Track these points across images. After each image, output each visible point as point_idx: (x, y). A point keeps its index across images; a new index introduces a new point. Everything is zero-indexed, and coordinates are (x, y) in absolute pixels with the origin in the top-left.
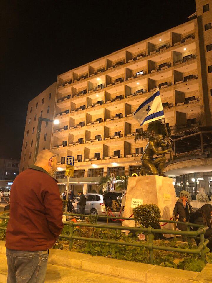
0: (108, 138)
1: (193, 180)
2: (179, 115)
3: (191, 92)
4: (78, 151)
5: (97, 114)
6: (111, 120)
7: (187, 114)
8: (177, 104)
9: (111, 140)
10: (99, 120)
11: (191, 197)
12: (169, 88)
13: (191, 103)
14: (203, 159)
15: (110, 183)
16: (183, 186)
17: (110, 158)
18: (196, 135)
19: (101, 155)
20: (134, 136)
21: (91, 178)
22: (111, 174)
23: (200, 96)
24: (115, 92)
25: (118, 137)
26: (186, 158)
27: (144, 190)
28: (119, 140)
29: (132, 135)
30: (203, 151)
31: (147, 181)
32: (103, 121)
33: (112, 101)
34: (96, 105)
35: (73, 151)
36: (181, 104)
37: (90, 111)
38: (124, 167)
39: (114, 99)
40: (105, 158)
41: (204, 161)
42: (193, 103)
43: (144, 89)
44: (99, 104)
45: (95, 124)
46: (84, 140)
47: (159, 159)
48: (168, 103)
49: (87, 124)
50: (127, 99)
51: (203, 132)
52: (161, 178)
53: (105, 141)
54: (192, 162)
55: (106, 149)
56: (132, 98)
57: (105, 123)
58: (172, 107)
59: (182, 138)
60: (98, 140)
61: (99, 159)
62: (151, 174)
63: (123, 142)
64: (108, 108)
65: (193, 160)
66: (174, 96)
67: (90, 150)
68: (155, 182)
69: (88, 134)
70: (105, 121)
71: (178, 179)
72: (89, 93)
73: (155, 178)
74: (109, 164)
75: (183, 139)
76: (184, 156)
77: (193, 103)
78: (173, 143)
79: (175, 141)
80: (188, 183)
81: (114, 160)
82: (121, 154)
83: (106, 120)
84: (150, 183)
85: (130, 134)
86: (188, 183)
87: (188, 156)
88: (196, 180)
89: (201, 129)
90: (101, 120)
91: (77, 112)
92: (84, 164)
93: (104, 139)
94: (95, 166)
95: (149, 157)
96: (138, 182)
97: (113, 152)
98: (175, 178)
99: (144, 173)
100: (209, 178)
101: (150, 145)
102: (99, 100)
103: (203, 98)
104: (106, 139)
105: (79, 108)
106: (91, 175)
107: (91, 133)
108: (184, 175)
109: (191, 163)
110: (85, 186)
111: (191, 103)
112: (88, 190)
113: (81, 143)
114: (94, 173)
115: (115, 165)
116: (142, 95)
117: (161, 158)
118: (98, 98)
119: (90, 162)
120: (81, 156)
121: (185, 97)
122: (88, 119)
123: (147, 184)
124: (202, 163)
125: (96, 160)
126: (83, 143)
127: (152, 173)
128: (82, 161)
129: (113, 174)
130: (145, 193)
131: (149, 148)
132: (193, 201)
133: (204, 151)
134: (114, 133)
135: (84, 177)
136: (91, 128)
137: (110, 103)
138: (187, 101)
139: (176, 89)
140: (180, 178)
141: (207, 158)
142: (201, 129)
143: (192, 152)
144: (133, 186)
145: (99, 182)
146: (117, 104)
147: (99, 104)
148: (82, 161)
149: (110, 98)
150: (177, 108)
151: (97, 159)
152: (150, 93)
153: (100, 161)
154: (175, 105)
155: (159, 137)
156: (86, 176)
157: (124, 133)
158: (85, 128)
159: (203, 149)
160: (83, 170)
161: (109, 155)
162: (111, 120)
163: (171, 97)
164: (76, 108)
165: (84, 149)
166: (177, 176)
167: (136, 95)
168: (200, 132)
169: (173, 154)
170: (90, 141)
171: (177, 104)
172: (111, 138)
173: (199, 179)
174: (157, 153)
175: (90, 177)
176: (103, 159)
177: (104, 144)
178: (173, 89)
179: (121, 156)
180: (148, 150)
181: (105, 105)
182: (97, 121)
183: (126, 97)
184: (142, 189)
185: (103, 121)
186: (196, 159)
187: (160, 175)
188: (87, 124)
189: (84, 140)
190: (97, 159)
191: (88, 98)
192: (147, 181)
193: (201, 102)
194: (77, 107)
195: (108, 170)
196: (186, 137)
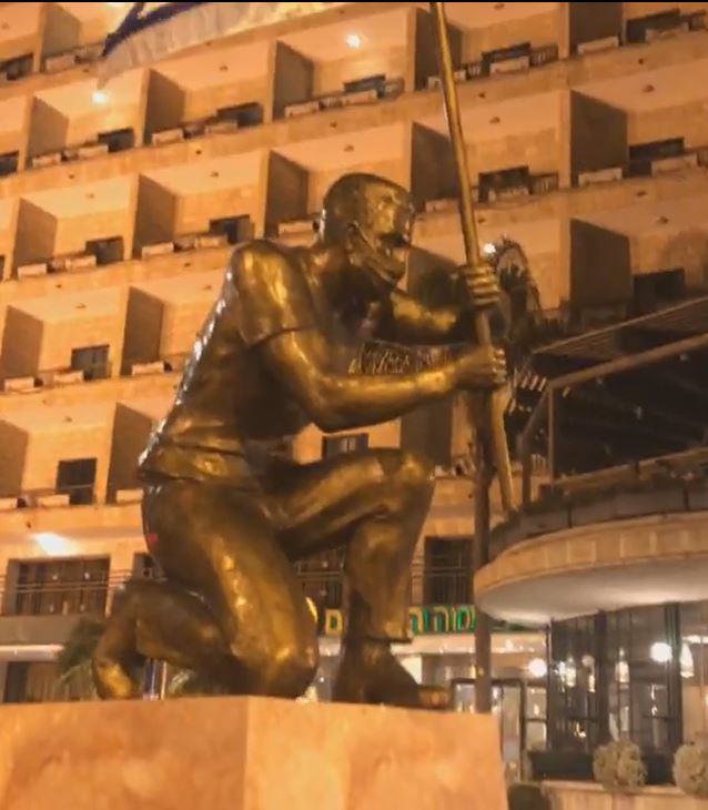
1: (660, 652)
2: (594, 249)
8: (582, 178)
10: (104, 252)
11: (638, 764)
12: (536, 74)
16: (592, 679)
24: (218, 79)
26: (622, 505)
35: (35, 432)
36: (605, 175)
37: (42, 186)
38: (104, 563)
42: (671, 173)
43: (392, 75)
44: (106, 148)
47: (339, 483)
49: (22, 271)
50: (283, 128)
54: (660, 534)
61: (81, 497)
62: (229, 674)
65: (670, 516)
70: (136, 254)
71: (562, 640)
72: (43, 70)
75: (609, 378)
76: (610, 493)
77: (671, 173)
78: (547, 399)
79: (558, 391)
80: (623, 669)
86: (623, 669)
87: (637, 490)
88: (677, 653)
93: (126, 372)
94: (52, 545)
95: (233, 445)
97: (56, 464)
98: (545, 629)
99: (147, 648)
102: (111, 124)
104: (137, 369)
108: (601, 618)
109: (653, 538)
114: (47, 589)
116: (375, 111)
118: (107, 111)
119: (19, 518)
125: (63, 506)
127: (236, 651)
132: (654, 789)
138: (639, 161)
140: (578, 633)
143: (661, 463)
145: (59, 653)
153: (84, 513)
154: (565, 181)
163: (544, 138)
166: (560, 617)
169: (540, 479)
174: (327, 391)
180: (226, 360)
188: (22, 271)
190: (65, 499)
191: (37, 108)
195: (16, 574)
196: (624, 362)
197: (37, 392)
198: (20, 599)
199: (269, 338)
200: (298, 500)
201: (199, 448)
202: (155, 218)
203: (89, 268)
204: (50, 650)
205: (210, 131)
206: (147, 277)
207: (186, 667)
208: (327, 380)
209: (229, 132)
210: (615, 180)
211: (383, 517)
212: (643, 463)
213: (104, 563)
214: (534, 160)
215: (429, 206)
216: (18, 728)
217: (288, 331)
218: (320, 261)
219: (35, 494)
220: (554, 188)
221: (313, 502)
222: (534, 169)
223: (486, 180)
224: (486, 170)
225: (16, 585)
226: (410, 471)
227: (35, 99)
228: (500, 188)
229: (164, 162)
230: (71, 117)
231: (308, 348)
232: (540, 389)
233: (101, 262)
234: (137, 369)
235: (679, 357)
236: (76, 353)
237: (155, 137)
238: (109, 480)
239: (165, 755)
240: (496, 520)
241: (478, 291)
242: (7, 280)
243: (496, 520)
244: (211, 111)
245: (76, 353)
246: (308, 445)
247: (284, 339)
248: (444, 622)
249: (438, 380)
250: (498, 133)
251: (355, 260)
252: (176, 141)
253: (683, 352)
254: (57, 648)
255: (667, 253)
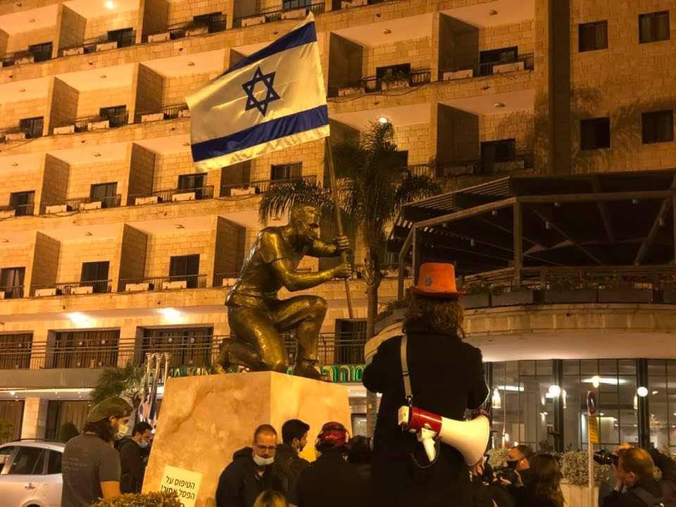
0: (148, 200)
2: (453, 124)
3: (507, 29)
4: (8, 250)
5: (105, 84)
6: (166, 117)
7: (480, 119)
9: (162, 208)
10: (114, 117)
13: (501, 74)
14: (519, 308)
15: (143, 398)
17: (151, 287)
18: (500, 210)
19: (114, 274)
20: (260, 199)
21: (61, 372)
22: (150, 357)
23: (538, 48)
25: (193, 195)
27: (222, 434)
28: (194, 211)
29: (252, 190)
30: (518, 277)
31: (238, 395)
32: (131, 120)
33: (174, 37)
34: (99, 46)
35: (66, 242)
36: (461, 74)
37: (70, 69)
38: (116, 333)
39: (185, 29)
40: (129, 287)
41: (520, 316)
44: (115, 44)
45: (92, 131)
46: (37, 199)
47: (294, 308)
48: (409, 65)
49: (56, 131)
51: (526, 198)
52: (299, 383)
53: (133, 212)
55: (135, 247)
56: (263, 28)
57: (139, 131)
58: (422, 83)
59: (445, 218)
60: (99, 204)
61: (100, 289)
62: (258, 366)
63: (213, 219)
64: (156, 65)
65: (480, 311)
66: (437, 39)
67: (63, 249)
68: (268, 398)
69: (55, 173)
70: (137, 120)
73: (268, 385)
74: (145, 311)
75: (450, 223)
78: (412, 234)
79: (420, 232)
81: (167, 295)
82: (202, 270)
83: (144, 118)
84: (246, 403)
85: (246, 187)
89: (520, 186)
90: (121, 117)
91: (9, 72)
92: (32, 306)
93: (131, 202)
94: (79, 321)
95: (259, 294)
96: (200, 396)
97: (168, 260)
99: (233, 361)
100: (541, 385)
101: (263, 246)
102: (116, 25)
103: (546, 59)
104: (138, 201)
105: (24, 52)
106: (61, 361)
107: (73, 172)
110: (31, 405)
111: (501, 74)
112: (43, 424)
113: (20, 213)
115: (171, 317)
117: (307, 304)
118: (113, 16)
119: (57, 303)
120: (22, 270)
121: (481, 49)
122: (63, 110)
123: (237, 407)
124: (510, 325)
125: (88, 294)
126: (32, 214)
127: (263, 361)
128: (21, 295)
129: (159, 358)
130: (223, 446)
131: (260, 260)
133: (524, 276)
134: (176, 179)
135: (28, 366)
136: (70, 146)
137: (166, 45)
138: (486, 63)
139: (444, 9)
141: (534, 307)
142: (520, 186)
143: (479, 277)
144: (181, 415)
145: (91, 394)
146: (192, 51)
147: (115, 44)
148: (21, 295)
149: (167, 19)
150: (447, 89)
151: (90, 289)
152: (339, 16)
153: (103, 298)
154: (434, 78)
155: (303, 214)
156: (37, 362)
157: (219, 182)
158: (42, 147)
159: (521, 266)
160: (26, 338)
161: (150, 275)
162: (166, 117)
163: (421, 44)
164: (8, 51)
165: (34, 242)
167: (279, 19)
168: (513, 200)
170: (64, 207)
171: (446, 76)
172: (160, 200)
173: (502, 388)
174: (291, 279)
175: (55, 365)
176: (121, 289)
177: (132, 224)
178: (435, 7)
179: (200, 279)
180: (257, 267)
181: (142, 49)
182: (100, 121)
183: (237, 24)
184: (214, 425)
185: (131, 120)
186: (490, 306)
187: (299, 372)
189: (37, 199)
190: (90, 289)
192: (238, 395)
193: (542, 68)
194: (11, 48)
195: (142, 337)
196: (460, 214)
197: (70, 215)
198: (56, 357)
199: (272, 262)
200: (281, 313)
201: (248, 295)
202: (150, 96)
203: (105, 129)
204: (84, 392)
205: (189, 36)
206: (145, 136)
207: (454, 260)
208: (291, 275)
209: (202, 35)
210: (468, 78)
211: (312, 320)
212: (466, 277)
213: (116, 333)
214: (415, 59)
215: (341, 93)
216: (197, 384)
217: (279, 259)
218: (289, 231)
219: (68, 285)
220: (427, 82)
221: (285, 314)
222: (414, 66)
223: (381, 72)
224: (381, 65)
225: (141, 346)
226: (319, 304)
227: (64, 6)
228: (390, 80)
229: (157, 55)
230: (88, 19)
231: (285, 264)
232: (409, 227)
233: (113, 125)
234: (138, 201)
235: (491, 212)
236: (94, 187)
237: (150, 38)
238: (120, 277)
239: (246, 389)
240: (381, 309)
241: (342, 245)
242: (45, 136)
243: (381, 309)
244: (189, 16)
245: (94, 187)
246: (283, 294)
247: (277, 262)
248: (347, 375)
249: (328, 274)
250: (390, 40)
251: (301, 232)
252: (165, 41)
253: (494, 209)
254: (88, 390)
255: (502, 127)
